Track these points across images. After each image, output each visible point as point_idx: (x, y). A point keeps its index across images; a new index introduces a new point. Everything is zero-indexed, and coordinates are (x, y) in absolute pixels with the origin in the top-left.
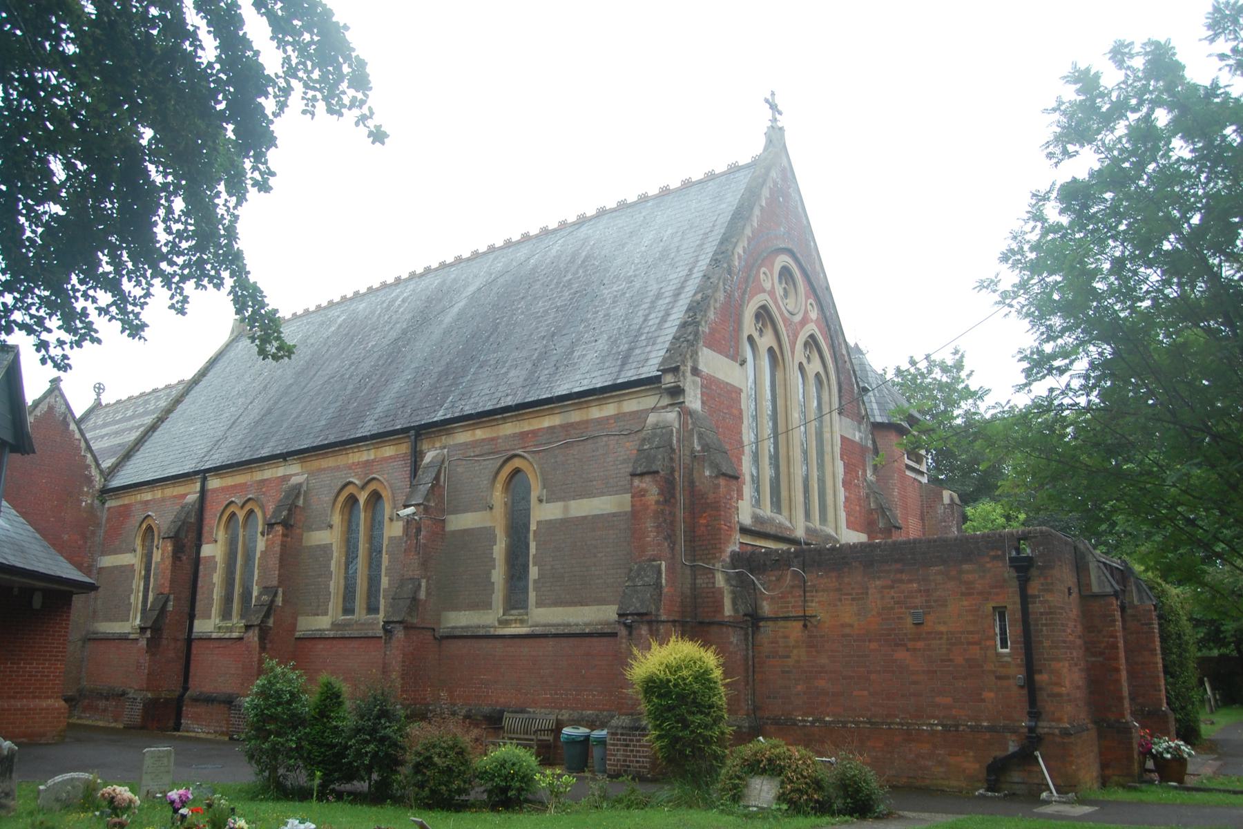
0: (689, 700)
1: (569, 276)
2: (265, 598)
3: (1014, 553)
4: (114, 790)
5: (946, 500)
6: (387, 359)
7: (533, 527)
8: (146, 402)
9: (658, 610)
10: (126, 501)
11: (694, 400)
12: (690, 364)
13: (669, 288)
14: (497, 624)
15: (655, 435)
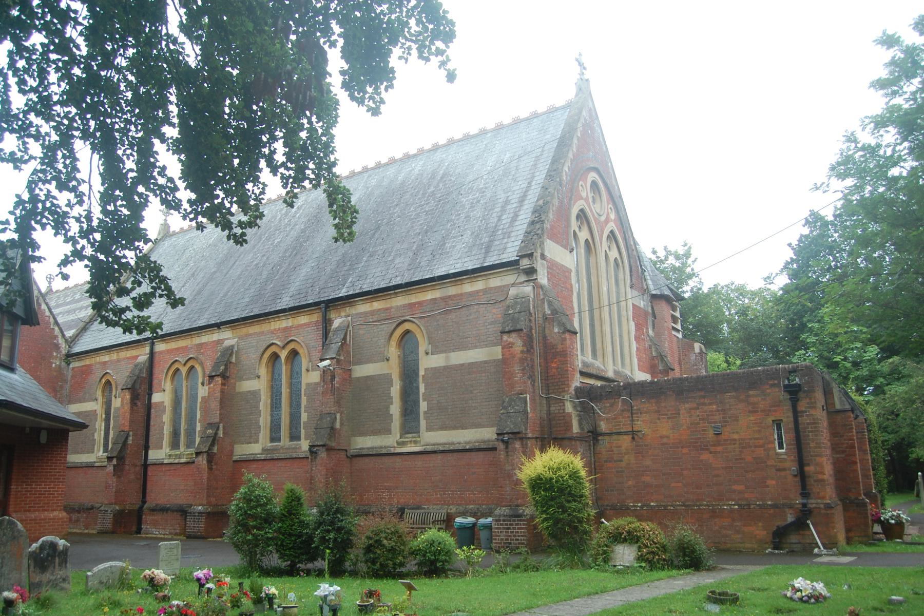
0: (566, 492)
1: (432, 189)
2: (209, 431)
3: (786, 382)
5: (697, 350)
6: (292, 252)
7: (303, 387)
9: (526, 430)
10: (87, 362)
11: (543, 278)
12: (539, 251)
13: (514, 196)
14: (396, 445)
15: (516, 303)
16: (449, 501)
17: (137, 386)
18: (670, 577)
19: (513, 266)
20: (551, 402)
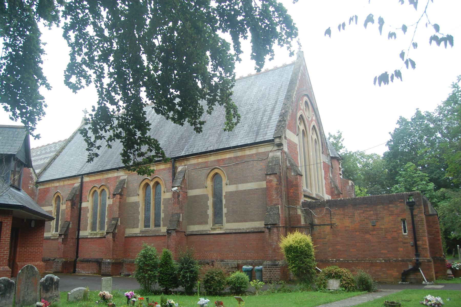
2: (113, 222)
3: (408, 201)
4: (104, 293)
6: (154, 133)
7: (224, 194)
8: (45, 149)
9: (279, 223)
10: (47, 186)
11: (285, 149)
12: (284, 135)
13: (269, 108)
14: (210, 230)
15: (273, 160)
16: (238, 258)
17: (74, 199)
18: (358, 295)
19: (271, 142)
20: (290, 209)
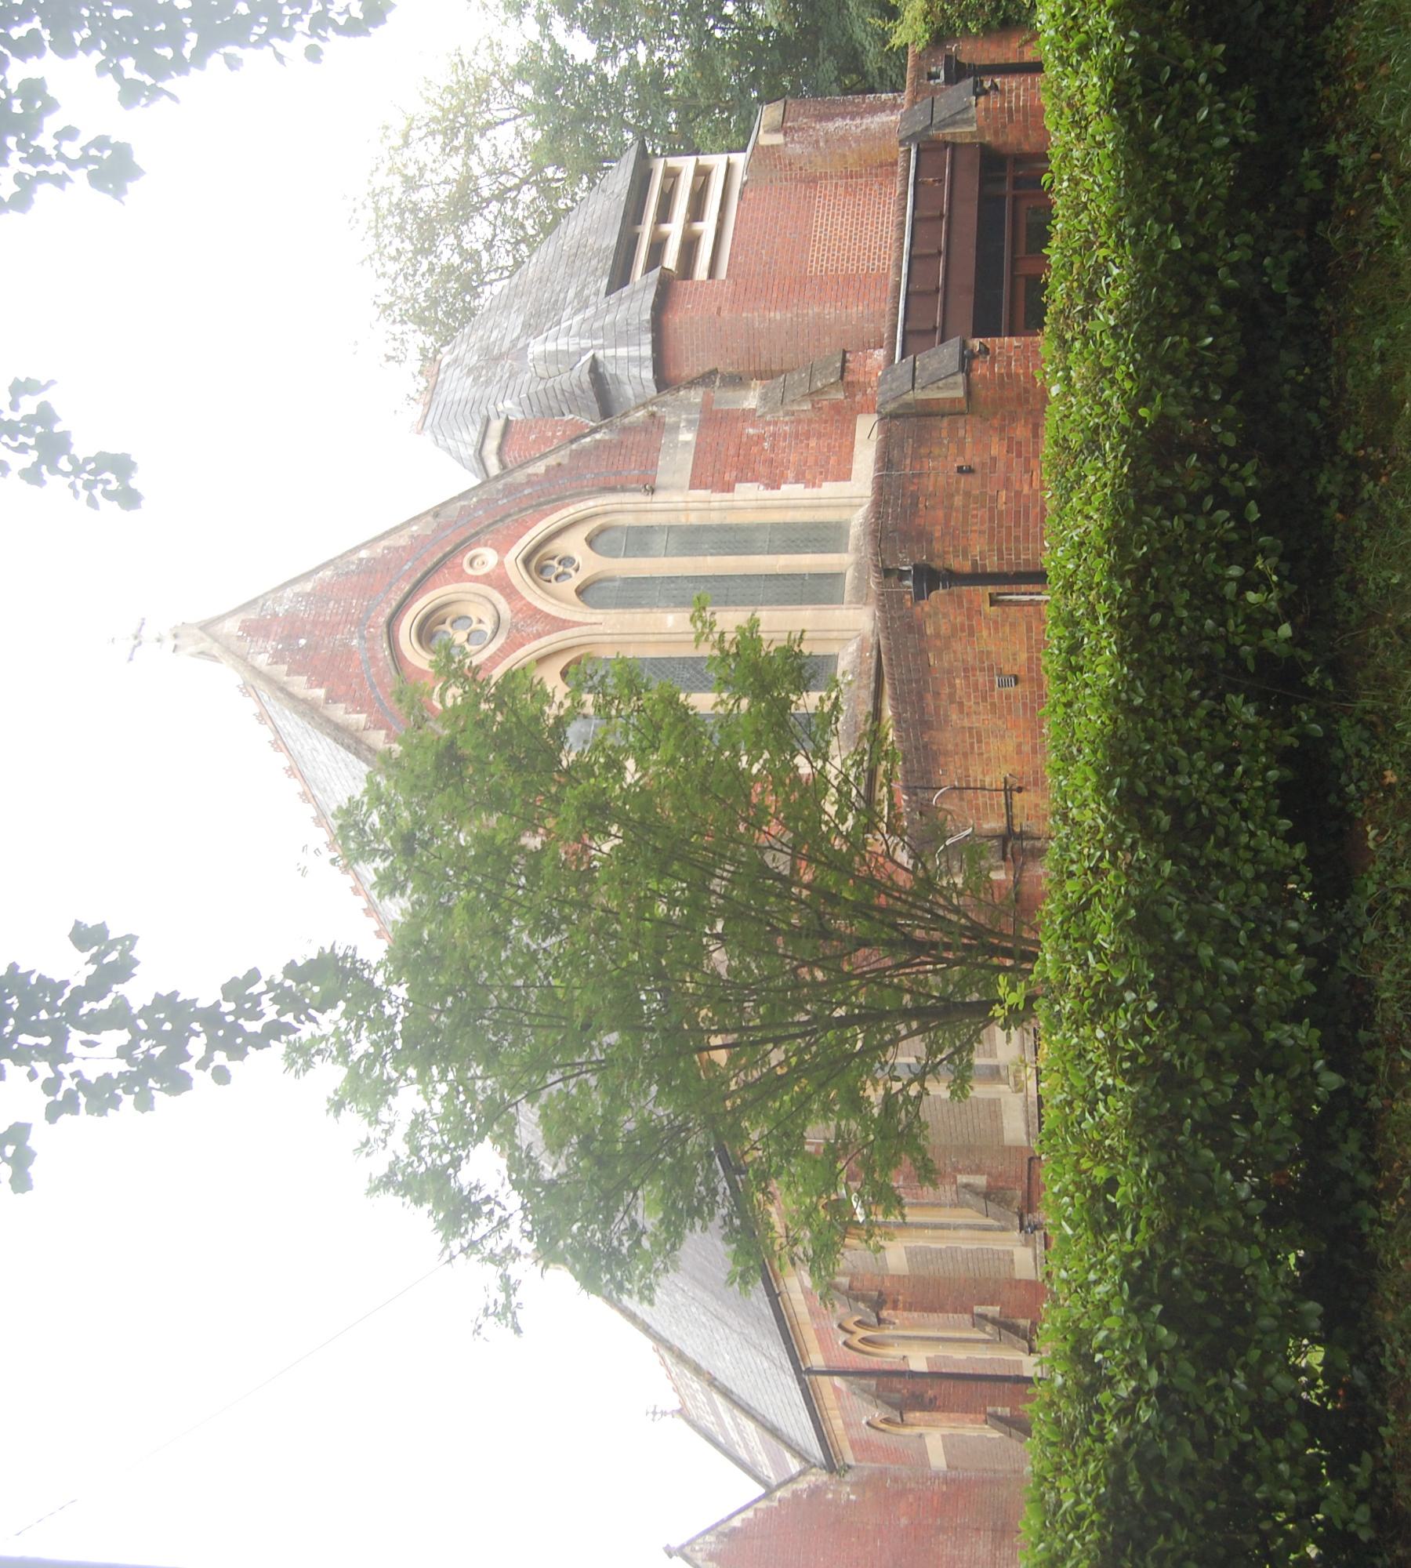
14: (1022, 1094)
17: (896, 1397)
